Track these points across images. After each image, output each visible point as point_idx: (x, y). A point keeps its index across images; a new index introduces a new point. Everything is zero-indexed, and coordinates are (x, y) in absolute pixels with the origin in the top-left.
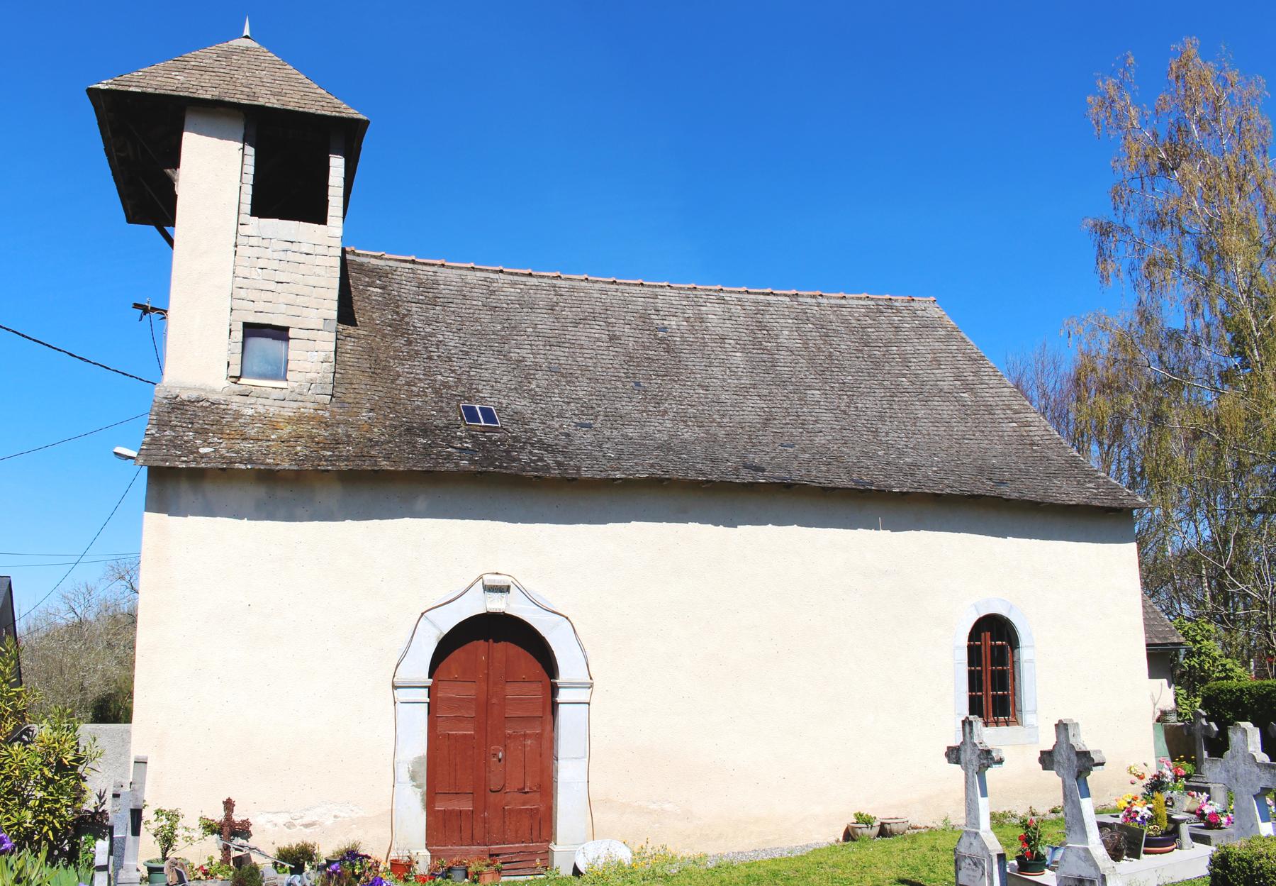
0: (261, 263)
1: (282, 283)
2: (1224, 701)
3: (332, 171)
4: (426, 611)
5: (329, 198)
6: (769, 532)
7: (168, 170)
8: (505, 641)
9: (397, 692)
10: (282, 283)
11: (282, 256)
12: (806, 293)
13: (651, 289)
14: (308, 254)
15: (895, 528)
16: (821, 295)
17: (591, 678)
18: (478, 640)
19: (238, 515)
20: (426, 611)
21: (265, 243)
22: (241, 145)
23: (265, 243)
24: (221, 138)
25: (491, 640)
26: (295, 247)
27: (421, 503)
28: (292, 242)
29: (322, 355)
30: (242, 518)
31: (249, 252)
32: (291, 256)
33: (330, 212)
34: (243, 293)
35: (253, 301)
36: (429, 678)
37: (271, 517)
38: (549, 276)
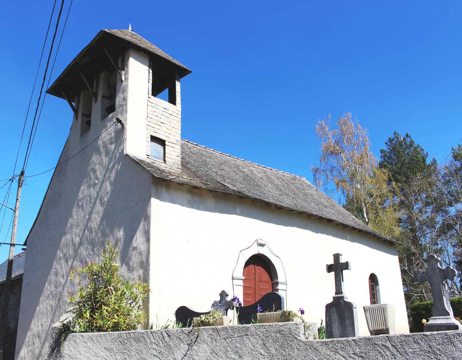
0: (156, 114)
1: (163, 123)
2: (421, 308)
3: (177, 86)
4: (242, 251)
5: (176, 96)
6: (325, 236)
7: (119, 70)
8: (259, 266)
9: (234, 281)
10: (163, 123)
11: (163, 113)
12: (274, 169)
13: (234, 159)
14: (171, 115)
15: (352, 241)
16: (278, 171)
17: (286, 281)
18: (252, 265)
19: (182, 205)
20: (242, 251)
21: (157, 107)
22: (148, 68)
23: (157, 107)
24: (142, 64)
25: (256, 265)
26: (167, 111)
27: (238, 210)
28: (165, 109)
29: (177, 154)
30: (184, 206)
31: (152, 109)
32: (165, 114)
33: (177, 101)
34: (150, 124)
35: (154, 128)
36: (243, 276)
37: (192, 207)
38: (202, 147)
